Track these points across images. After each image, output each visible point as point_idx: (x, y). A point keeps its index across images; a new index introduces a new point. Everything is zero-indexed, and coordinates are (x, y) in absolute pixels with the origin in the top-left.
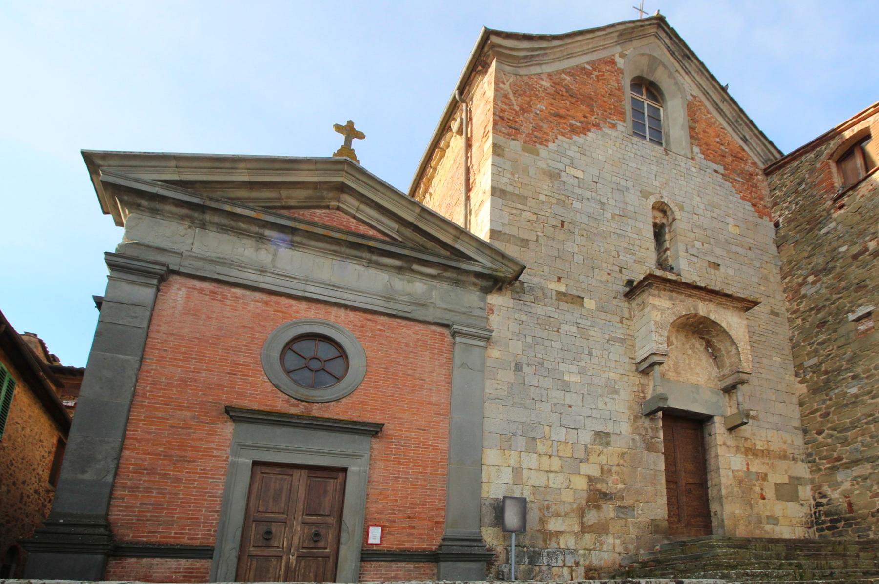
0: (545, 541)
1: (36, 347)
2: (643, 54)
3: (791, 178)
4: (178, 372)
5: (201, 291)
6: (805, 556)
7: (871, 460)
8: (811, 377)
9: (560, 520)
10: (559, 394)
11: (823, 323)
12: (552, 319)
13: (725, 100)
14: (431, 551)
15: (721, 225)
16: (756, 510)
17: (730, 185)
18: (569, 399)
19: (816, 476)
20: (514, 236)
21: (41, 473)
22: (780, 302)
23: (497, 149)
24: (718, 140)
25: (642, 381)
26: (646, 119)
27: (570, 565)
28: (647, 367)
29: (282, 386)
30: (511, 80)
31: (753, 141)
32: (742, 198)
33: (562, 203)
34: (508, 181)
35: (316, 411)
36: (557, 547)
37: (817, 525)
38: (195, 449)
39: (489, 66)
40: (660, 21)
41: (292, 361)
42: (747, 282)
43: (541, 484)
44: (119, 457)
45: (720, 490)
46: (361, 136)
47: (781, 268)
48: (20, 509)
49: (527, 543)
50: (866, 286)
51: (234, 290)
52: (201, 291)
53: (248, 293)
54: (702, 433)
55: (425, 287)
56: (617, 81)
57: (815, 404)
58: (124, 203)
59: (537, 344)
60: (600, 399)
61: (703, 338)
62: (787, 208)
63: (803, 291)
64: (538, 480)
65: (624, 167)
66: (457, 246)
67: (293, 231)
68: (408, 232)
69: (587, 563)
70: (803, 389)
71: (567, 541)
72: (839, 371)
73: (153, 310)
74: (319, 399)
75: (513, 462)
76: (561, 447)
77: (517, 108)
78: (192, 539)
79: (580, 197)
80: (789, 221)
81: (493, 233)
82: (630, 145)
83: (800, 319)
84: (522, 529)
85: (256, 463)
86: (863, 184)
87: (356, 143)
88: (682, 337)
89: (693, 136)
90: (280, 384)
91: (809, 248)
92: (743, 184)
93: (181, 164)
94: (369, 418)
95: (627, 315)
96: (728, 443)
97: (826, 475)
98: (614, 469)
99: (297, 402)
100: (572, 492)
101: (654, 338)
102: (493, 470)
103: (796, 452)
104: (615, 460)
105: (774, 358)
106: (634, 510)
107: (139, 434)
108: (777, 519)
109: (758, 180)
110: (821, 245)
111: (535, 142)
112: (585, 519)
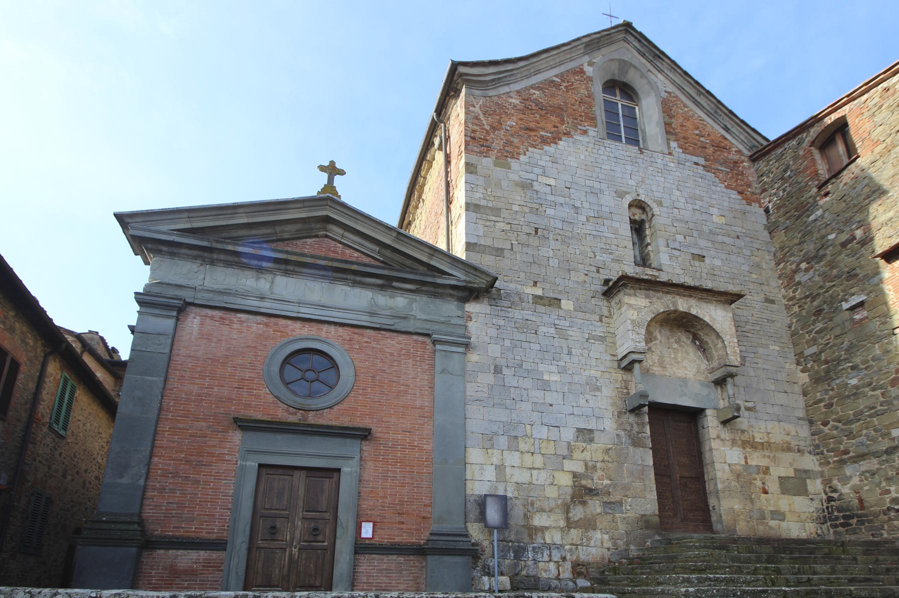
0: (530, 536)
1: (98, 343)
2: (612, 60)
3: (777, 165)
4: (195, 389)
5: (212, 318)
6: (790, 559)
7: (877, 455)
8: (812, 366)
9: (545, 515)
10: (539, 394)
11: (819, 312)
12: (529, 322)
13: (702, 93)
14: (420, 545)
15: (705, 217)
16: (758, 505)
17: (713, 175)
18: (550, 397)
19: (826, 469)
20: (489, 246)
21: (100, 461)
22: (776, 289)
23: (470, 168)
24: (697, 132)
25: (625, 377)
26: (621, 120)
27: (556, 560)
28: (628, 365)
29: (282, 397)
30: (481, 103)
31: (735, 129)
32: (726, 187)
33: (535, 211)
34: (482, 196)
35: (312, 418)
36: (542, 541)
37: (830, 520)
38: (211, 455)
39: (460, 91)
40: (627, 27)
41: (292, 373)
42: (736, 271)
43: (525, 481)
44: (149, 464)
45: (716, 484)
46: (342, 173)
47: (774, 254)
48: (83, 494)
49: (513, 537)
50: (857, 275)
51: (239, 315)
52: (212, 318)
53: (251, 317)
54: (696, 425)
55: (406, 300)
56: (587, 88)
57: (818, 394)
58: (150, 250)
59: (516, 346)
60: (581, 396)
61: (689, 332)
62: (775, 194)
63: (797, 278)
64: (523, 477)
65: (598, 170)
66: (433, 263)
67: (286, 262)
68: (388, 253)
69: (574, 558)
70: (804, 378)
71: (552, 537)
72: (838, 361)
73: (174, 336)
74: (313, 407)
75: (495, 460)
76: (544, 445)
77: (488, 127)
78: (209, 533)
79: (553, 204)
80: (778, 208)
81: (469, 246)
82: (603, 148)
83: (797, 307)
84: (505, 525)
85: (261, 466)
86: (845, 173)
87: (337, 178)
88: (666, 332)
89: (669, 131)
90: (279, 395)
91: (800, 235)
92: (727, 173)
93: (192, 215)
94: (359, 423)
95: (606, 313)
96: (723, 437)
97: (834, 468)
98: (599, 465)
99: (294, 410)
100: (556, 488)
101: (631, 337)
102: (476, 468)
103: (802, 443)
104: (599, 456)
105: (771, 347)
106: (621, 505)
107: (165, 443)
108: (783, 514)
109: (744, 167)
110: (810, 232)
111: (506, 156)
112: (570, 515)
